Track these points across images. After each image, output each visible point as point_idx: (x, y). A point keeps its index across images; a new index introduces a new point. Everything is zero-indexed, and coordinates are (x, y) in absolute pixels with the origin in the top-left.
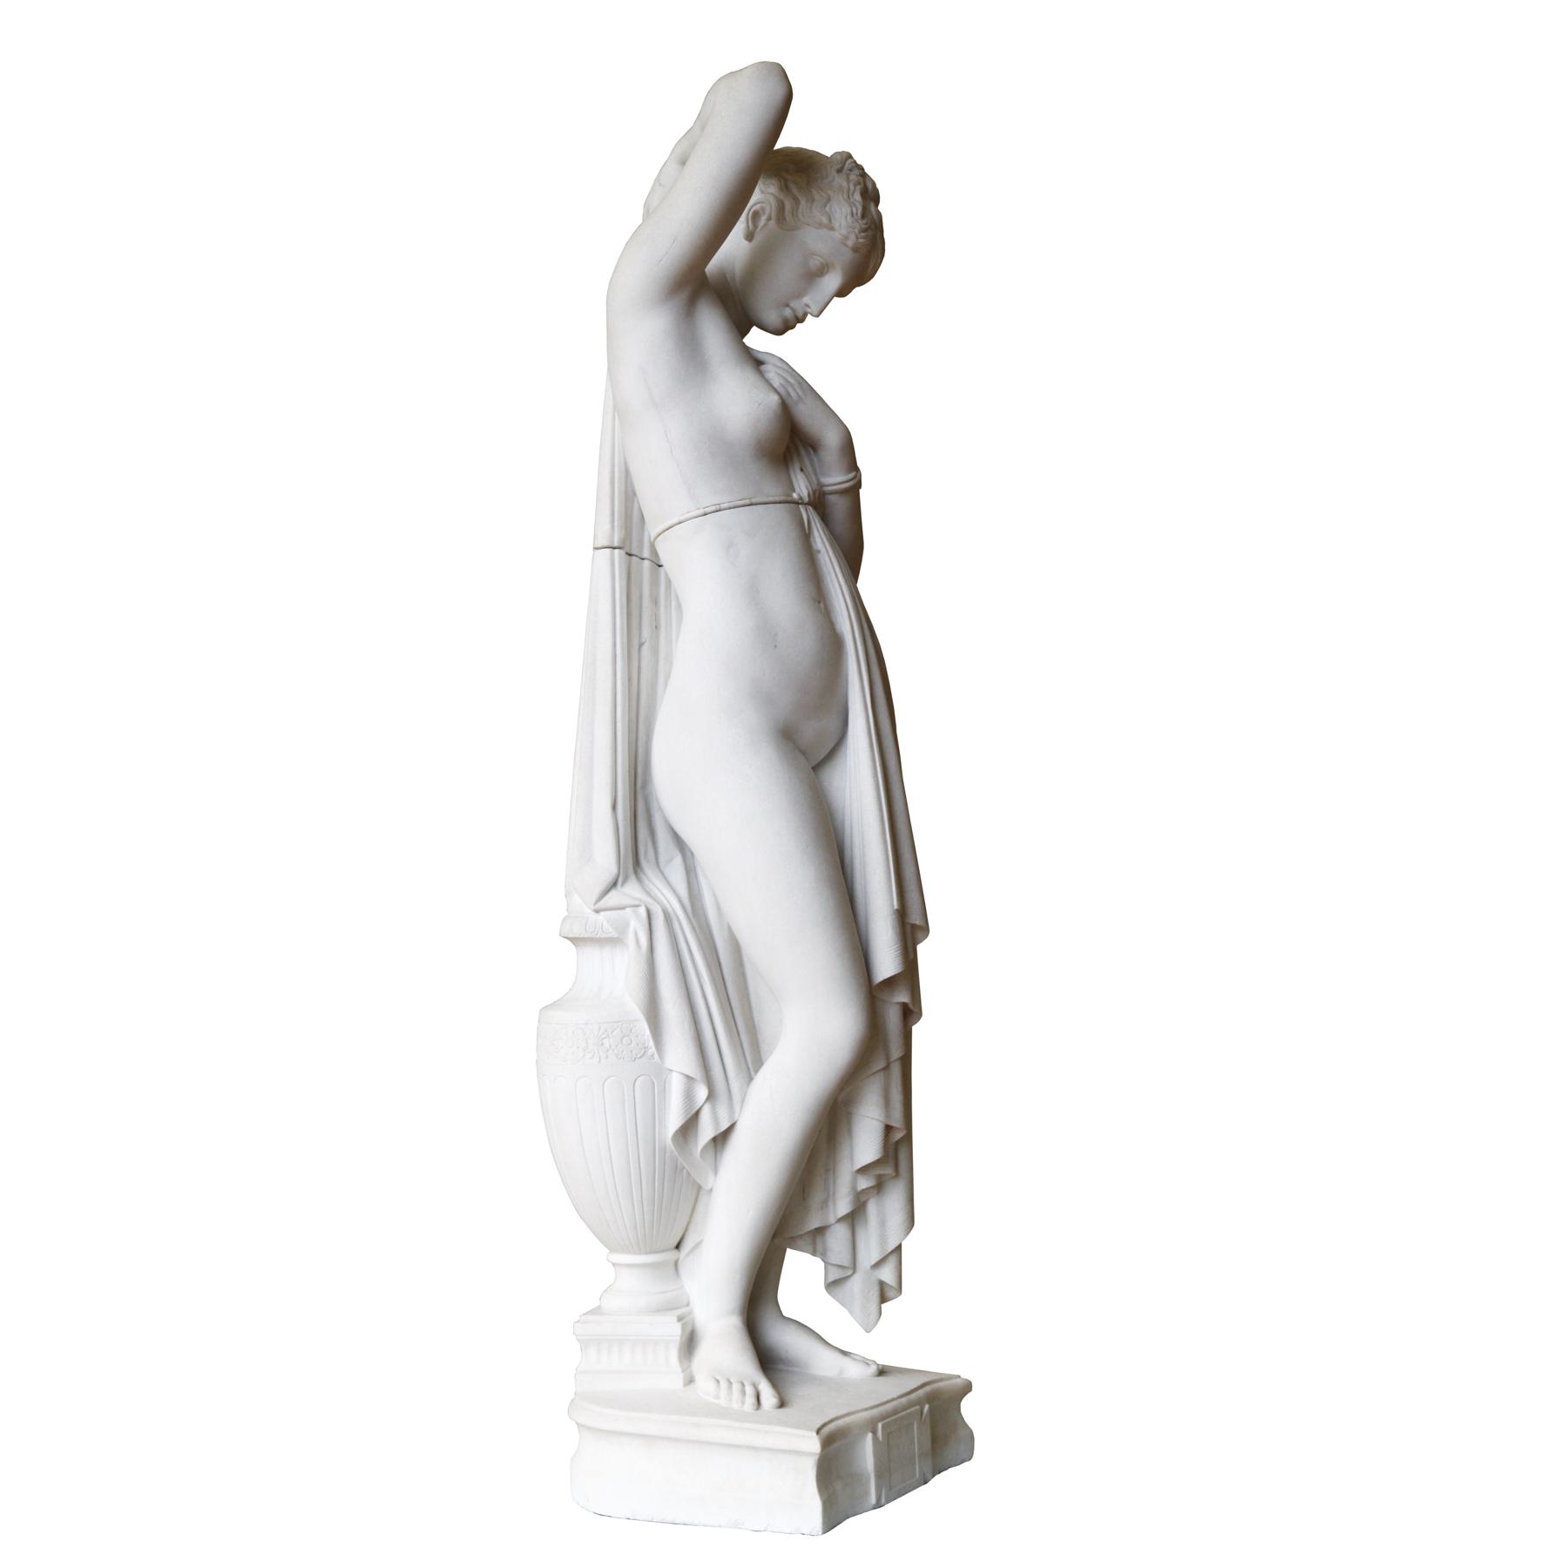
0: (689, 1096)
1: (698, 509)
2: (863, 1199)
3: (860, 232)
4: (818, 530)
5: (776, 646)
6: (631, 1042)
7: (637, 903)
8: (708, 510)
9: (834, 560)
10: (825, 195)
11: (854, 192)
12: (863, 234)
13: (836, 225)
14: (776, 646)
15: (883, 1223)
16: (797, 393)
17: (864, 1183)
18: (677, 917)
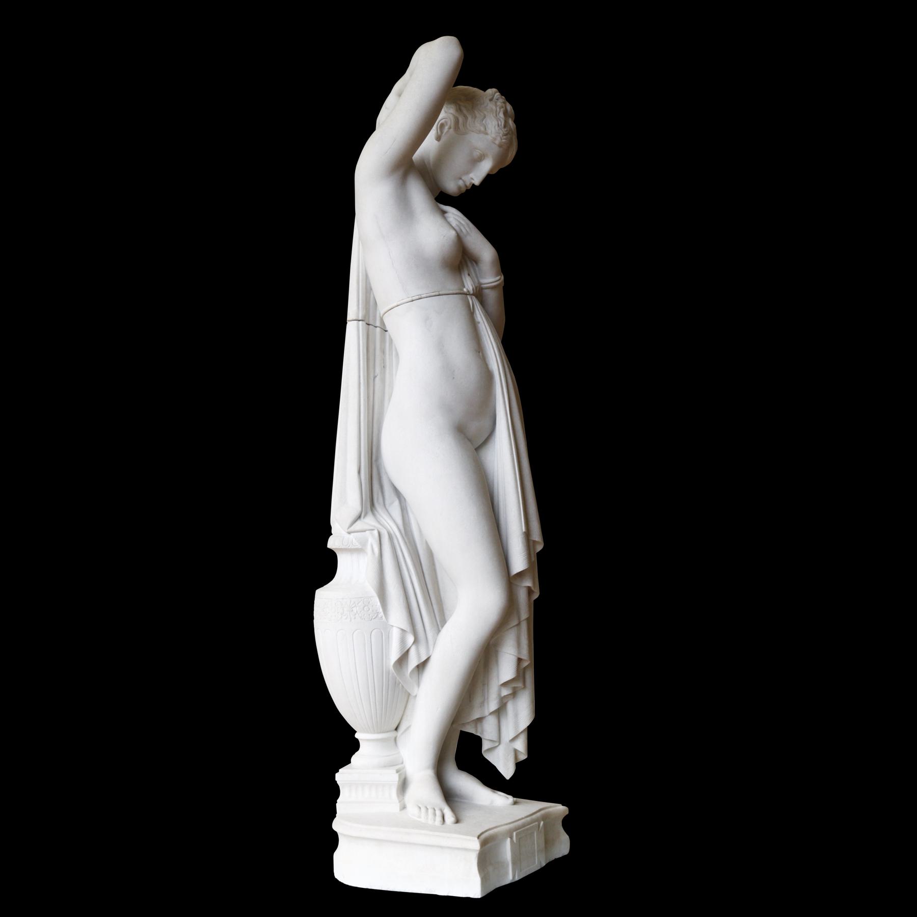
0: (403, 641)
1: (408, 298)
2: (505, 701)
3: (503, 136)
4: (478, 310)
5: (454, 378)
6: (369, 609)
8: (414, 298)
9: (488, 328)
10: (482, 114)
11: (499, 112)
12: (505, 137)
13: (489, 132)
14: (454, 378)
15: (516, 715)
16: (466, 230)
17: (505, 692)
18: (396, 536)
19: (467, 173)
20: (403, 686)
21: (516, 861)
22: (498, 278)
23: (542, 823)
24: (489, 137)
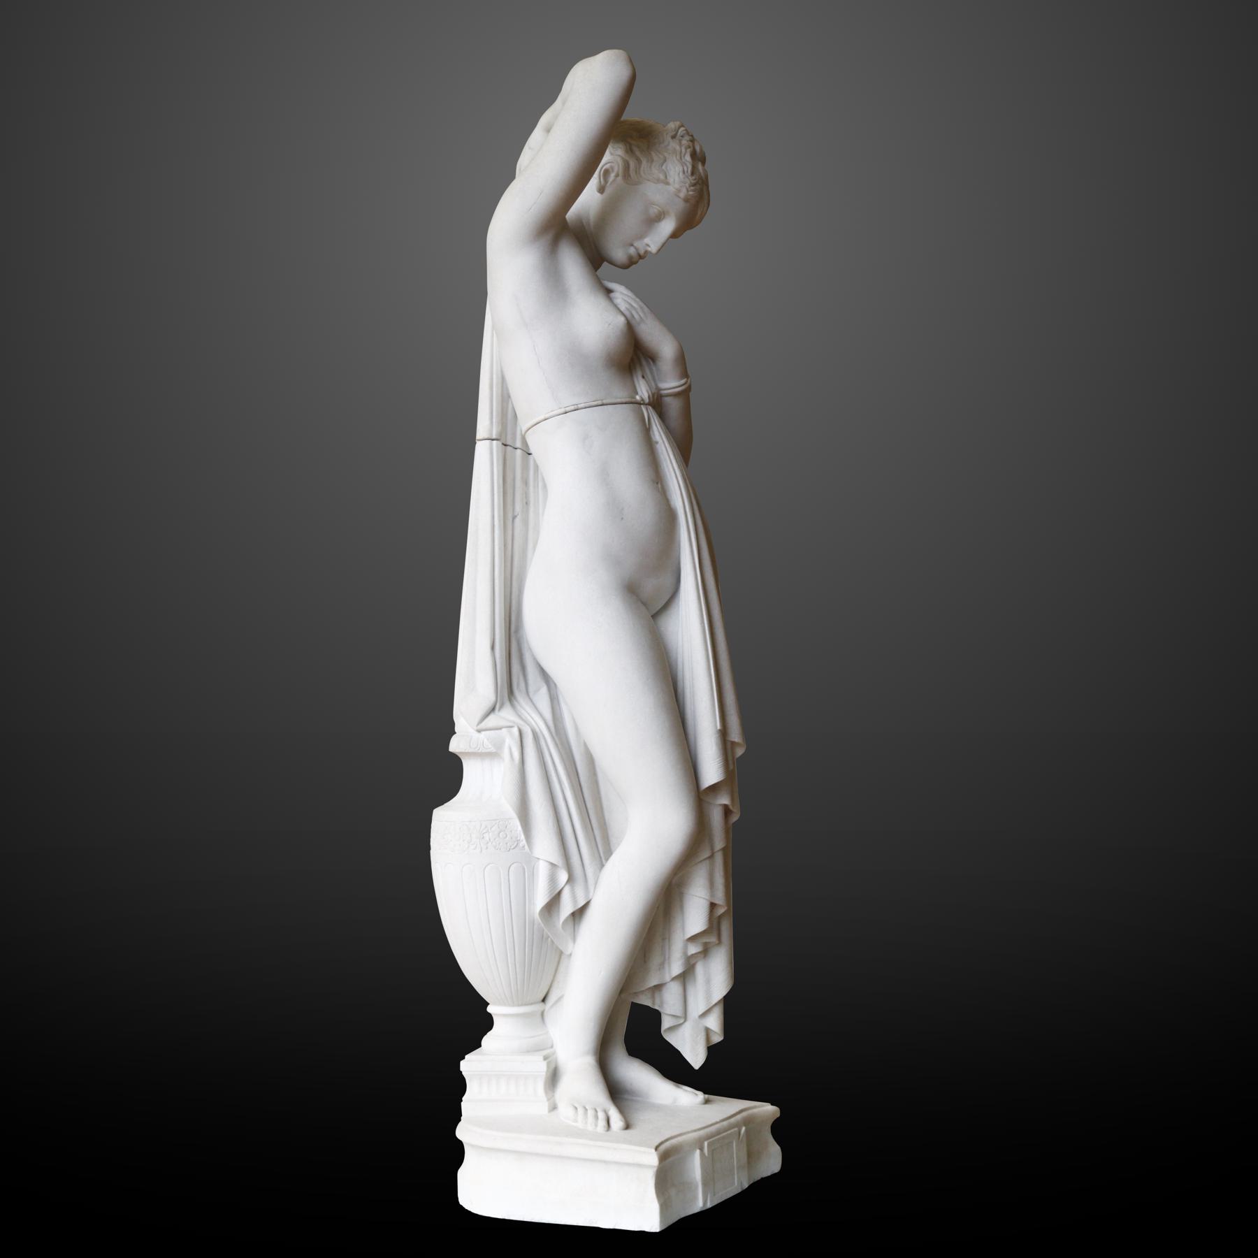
0: (553, 879)
1: (560, 408)
2: (692, 962)
3: (690, 187)
4: (656, 425)
5: (622, 519)
6: (506, 836)
8: (568, 409)
9: (669, 449)
10: (662, 157)
11: (685, 154)
12: (692, 188)
14: (622, 519)
15: (708, 981)
16: (640, 316)
17: (693, 949)
18: (543, 736)
19: (641, 237)
21: (708, 1181)
22: (683, 381)
24: (671, 189)
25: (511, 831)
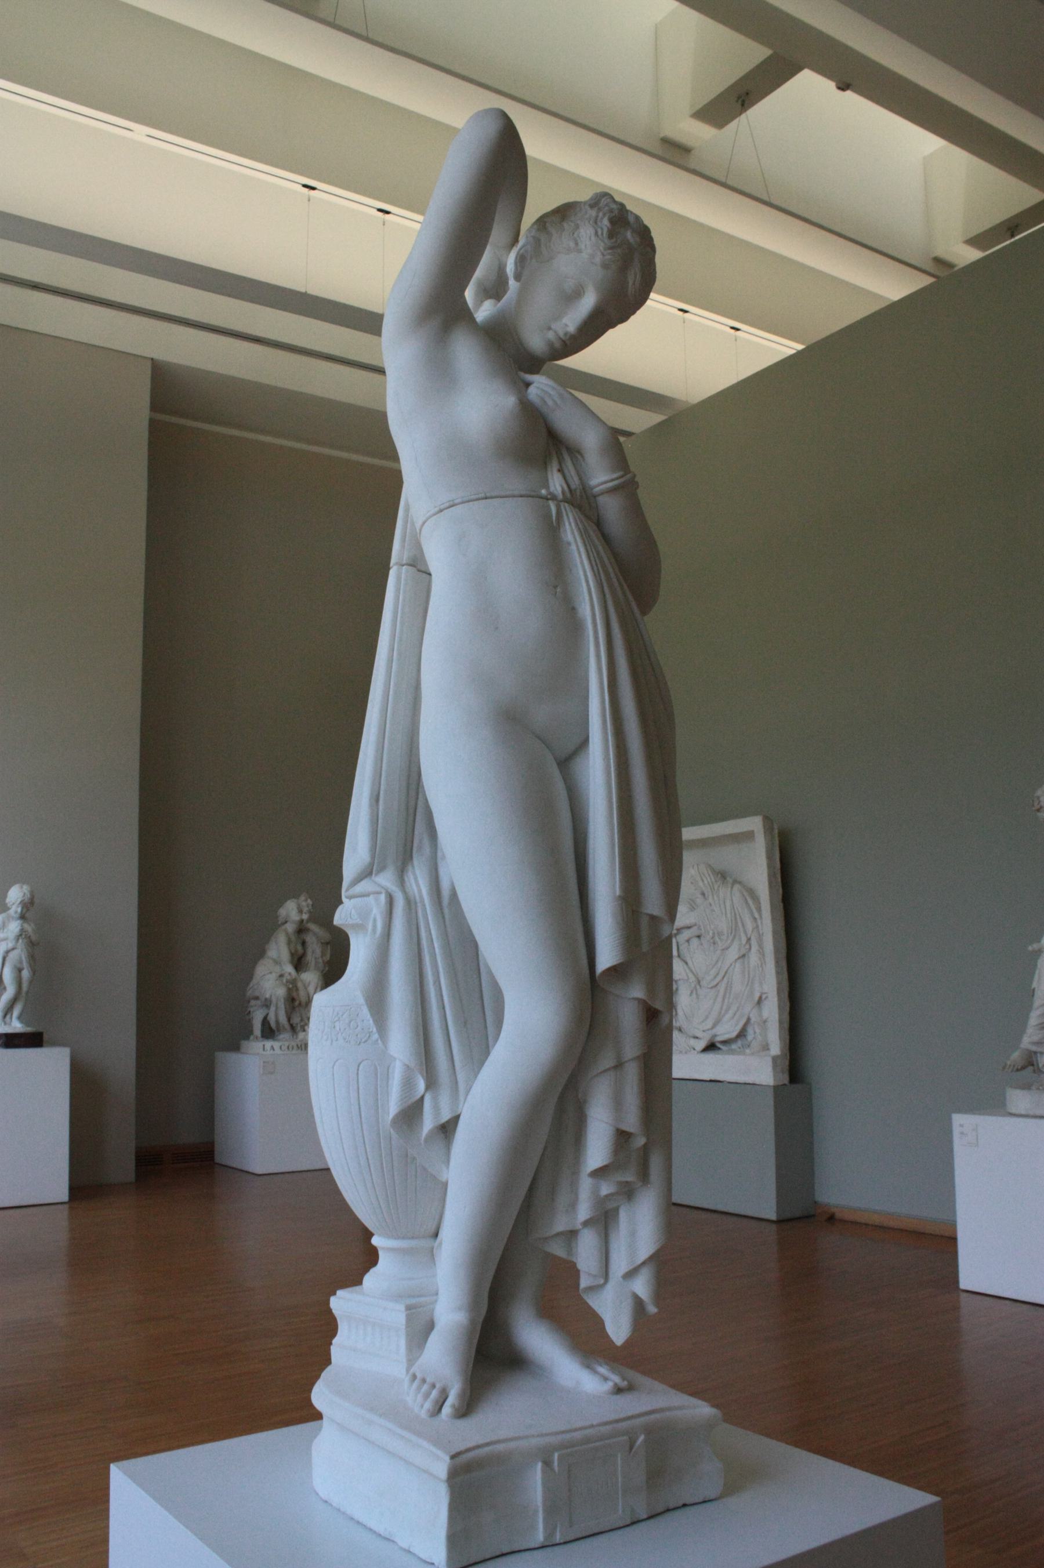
0: (408, 1084)
1: (436, 507)
2: (611, 1205)
4: (570, 524)
6: (358, 1026)
7: (378, 889)
8: (442, 507)
9: (582, 550)
10: (573, 224)
11: (602, 219)
12: (610, 251)
14: (497, 628)
15: (633, 1234)
17: (606, 1189)
18: (424, 905)
19: (557, 318)
20: (425, 1169)
23: (642, 1438)
24: (585, 255)
25: (363, 1021)
